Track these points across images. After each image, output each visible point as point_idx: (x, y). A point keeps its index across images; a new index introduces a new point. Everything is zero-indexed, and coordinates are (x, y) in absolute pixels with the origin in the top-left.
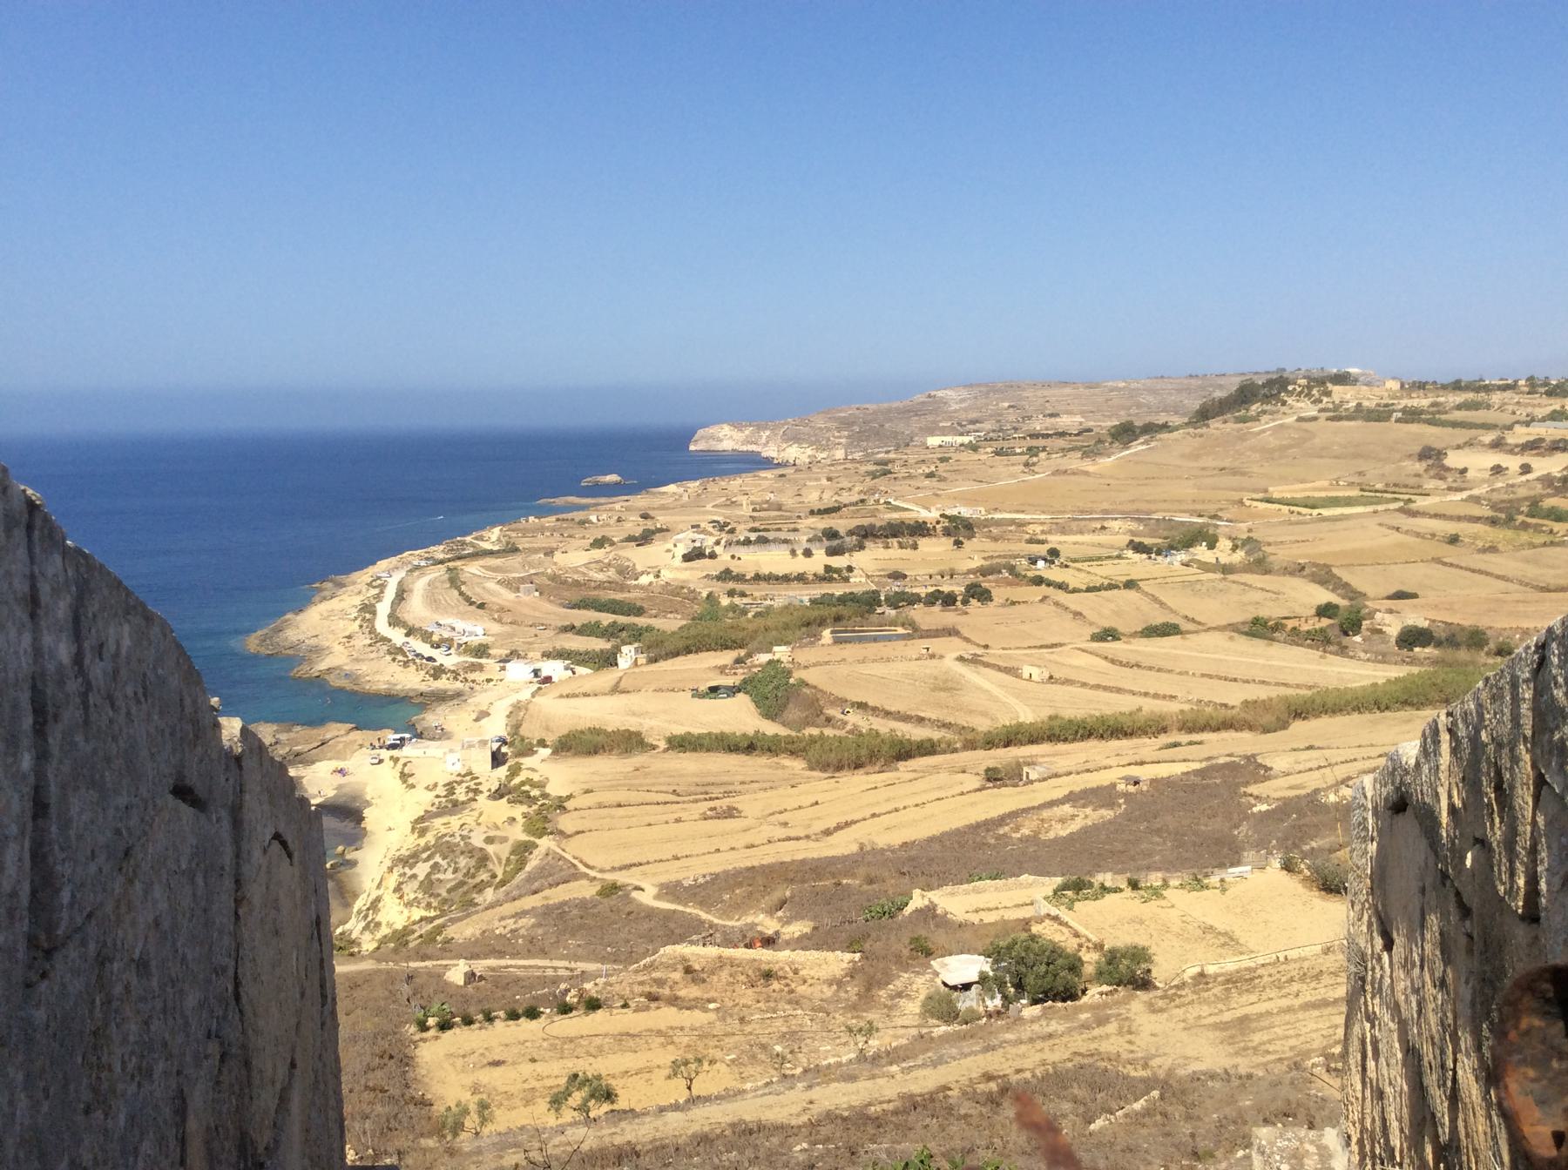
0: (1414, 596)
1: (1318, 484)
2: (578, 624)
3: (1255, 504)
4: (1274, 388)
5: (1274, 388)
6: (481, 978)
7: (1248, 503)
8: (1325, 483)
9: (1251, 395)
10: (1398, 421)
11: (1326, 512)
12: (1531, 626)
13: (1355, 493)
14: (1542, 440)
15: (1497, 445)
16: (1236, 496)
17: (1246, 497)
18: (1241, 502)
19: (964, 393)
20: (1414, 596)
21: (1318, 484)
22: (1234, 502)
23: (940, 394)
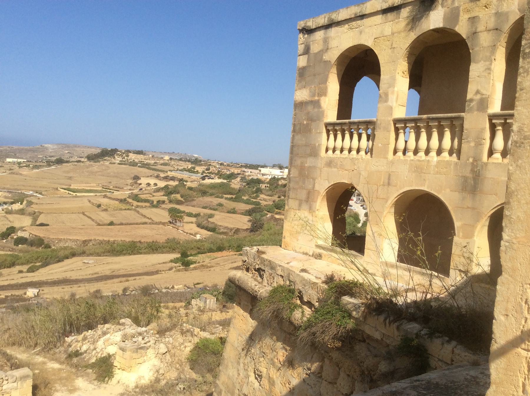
0: (48, 225)
1: (92, 185)
2: (194, 213)
3: (61, 190)
4: (112, 153)
5: (112, 153)
6: (102, 297)
7: (59, 189)
8: (95, 185)
9: (107, 153)
10: (139, 167)
11: (78, 194)
12: (63, 238)
13: (100, 189)
14: (168, 176)
15: (157, 177)
16: (56, 186)
17: (59, 187)
18: (57, 189)
19: (55, 147)
20: (48, 225)
21: (92, 185)
22: (54, 188)
23: (46, 145)
